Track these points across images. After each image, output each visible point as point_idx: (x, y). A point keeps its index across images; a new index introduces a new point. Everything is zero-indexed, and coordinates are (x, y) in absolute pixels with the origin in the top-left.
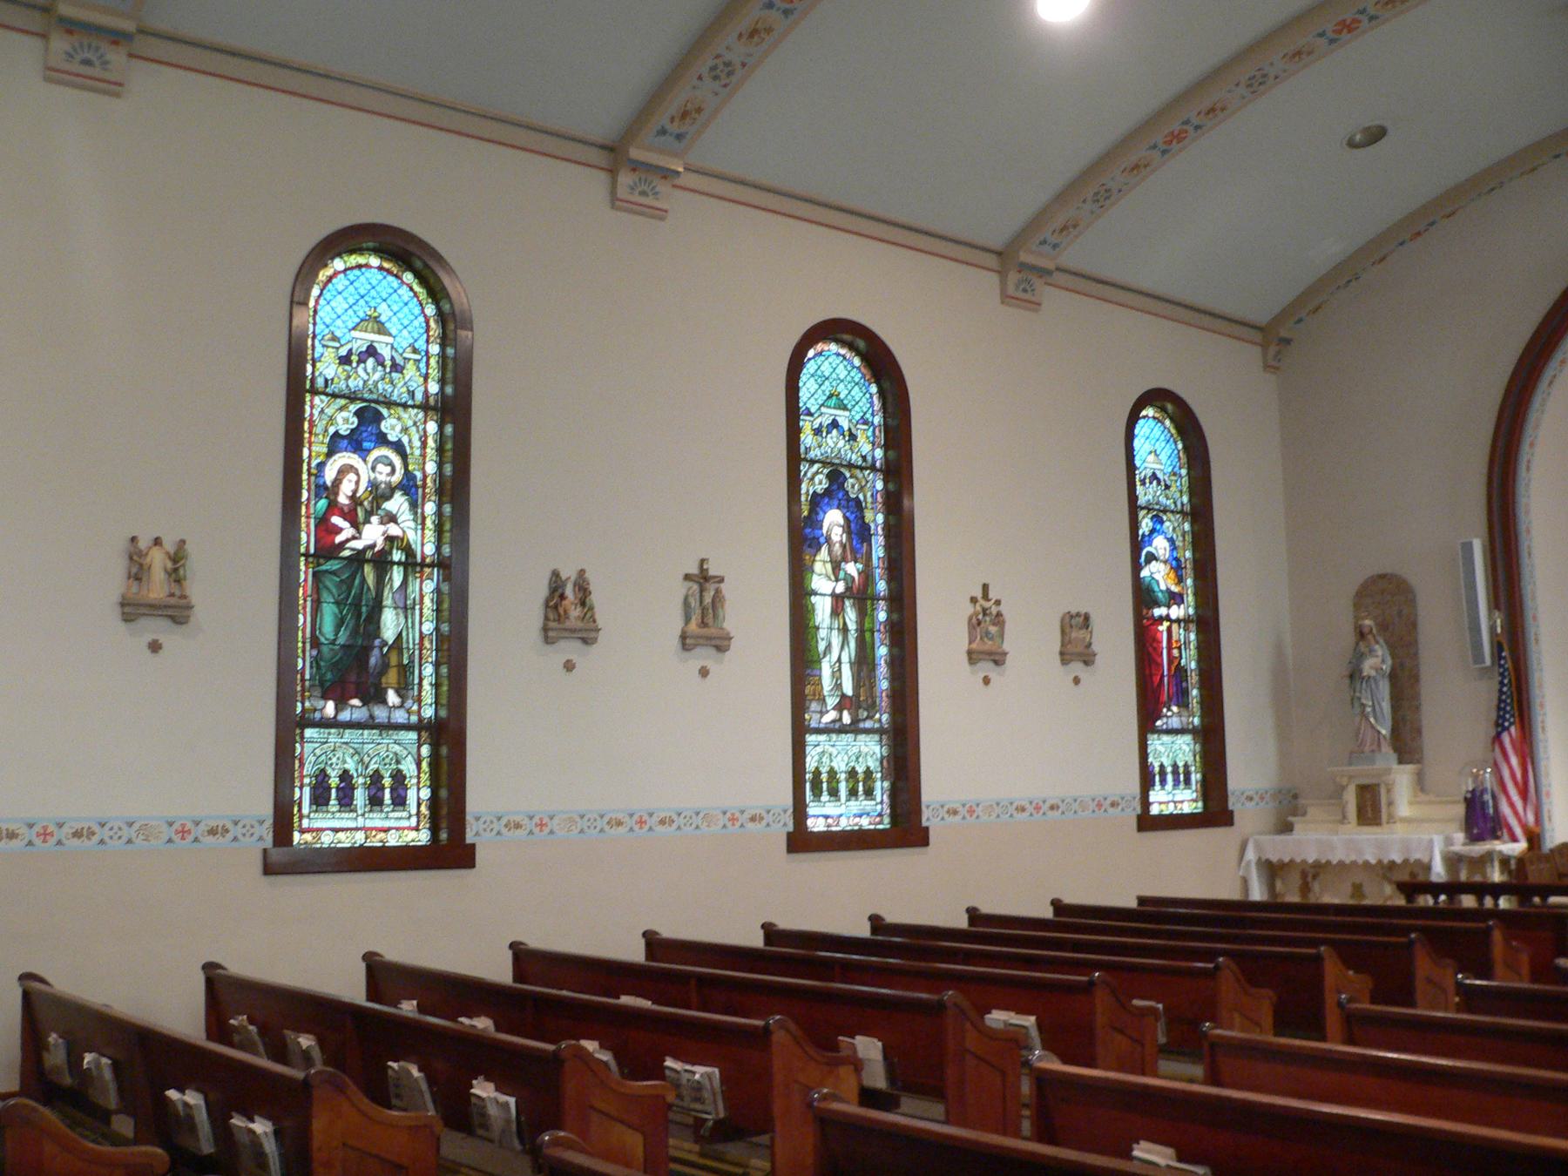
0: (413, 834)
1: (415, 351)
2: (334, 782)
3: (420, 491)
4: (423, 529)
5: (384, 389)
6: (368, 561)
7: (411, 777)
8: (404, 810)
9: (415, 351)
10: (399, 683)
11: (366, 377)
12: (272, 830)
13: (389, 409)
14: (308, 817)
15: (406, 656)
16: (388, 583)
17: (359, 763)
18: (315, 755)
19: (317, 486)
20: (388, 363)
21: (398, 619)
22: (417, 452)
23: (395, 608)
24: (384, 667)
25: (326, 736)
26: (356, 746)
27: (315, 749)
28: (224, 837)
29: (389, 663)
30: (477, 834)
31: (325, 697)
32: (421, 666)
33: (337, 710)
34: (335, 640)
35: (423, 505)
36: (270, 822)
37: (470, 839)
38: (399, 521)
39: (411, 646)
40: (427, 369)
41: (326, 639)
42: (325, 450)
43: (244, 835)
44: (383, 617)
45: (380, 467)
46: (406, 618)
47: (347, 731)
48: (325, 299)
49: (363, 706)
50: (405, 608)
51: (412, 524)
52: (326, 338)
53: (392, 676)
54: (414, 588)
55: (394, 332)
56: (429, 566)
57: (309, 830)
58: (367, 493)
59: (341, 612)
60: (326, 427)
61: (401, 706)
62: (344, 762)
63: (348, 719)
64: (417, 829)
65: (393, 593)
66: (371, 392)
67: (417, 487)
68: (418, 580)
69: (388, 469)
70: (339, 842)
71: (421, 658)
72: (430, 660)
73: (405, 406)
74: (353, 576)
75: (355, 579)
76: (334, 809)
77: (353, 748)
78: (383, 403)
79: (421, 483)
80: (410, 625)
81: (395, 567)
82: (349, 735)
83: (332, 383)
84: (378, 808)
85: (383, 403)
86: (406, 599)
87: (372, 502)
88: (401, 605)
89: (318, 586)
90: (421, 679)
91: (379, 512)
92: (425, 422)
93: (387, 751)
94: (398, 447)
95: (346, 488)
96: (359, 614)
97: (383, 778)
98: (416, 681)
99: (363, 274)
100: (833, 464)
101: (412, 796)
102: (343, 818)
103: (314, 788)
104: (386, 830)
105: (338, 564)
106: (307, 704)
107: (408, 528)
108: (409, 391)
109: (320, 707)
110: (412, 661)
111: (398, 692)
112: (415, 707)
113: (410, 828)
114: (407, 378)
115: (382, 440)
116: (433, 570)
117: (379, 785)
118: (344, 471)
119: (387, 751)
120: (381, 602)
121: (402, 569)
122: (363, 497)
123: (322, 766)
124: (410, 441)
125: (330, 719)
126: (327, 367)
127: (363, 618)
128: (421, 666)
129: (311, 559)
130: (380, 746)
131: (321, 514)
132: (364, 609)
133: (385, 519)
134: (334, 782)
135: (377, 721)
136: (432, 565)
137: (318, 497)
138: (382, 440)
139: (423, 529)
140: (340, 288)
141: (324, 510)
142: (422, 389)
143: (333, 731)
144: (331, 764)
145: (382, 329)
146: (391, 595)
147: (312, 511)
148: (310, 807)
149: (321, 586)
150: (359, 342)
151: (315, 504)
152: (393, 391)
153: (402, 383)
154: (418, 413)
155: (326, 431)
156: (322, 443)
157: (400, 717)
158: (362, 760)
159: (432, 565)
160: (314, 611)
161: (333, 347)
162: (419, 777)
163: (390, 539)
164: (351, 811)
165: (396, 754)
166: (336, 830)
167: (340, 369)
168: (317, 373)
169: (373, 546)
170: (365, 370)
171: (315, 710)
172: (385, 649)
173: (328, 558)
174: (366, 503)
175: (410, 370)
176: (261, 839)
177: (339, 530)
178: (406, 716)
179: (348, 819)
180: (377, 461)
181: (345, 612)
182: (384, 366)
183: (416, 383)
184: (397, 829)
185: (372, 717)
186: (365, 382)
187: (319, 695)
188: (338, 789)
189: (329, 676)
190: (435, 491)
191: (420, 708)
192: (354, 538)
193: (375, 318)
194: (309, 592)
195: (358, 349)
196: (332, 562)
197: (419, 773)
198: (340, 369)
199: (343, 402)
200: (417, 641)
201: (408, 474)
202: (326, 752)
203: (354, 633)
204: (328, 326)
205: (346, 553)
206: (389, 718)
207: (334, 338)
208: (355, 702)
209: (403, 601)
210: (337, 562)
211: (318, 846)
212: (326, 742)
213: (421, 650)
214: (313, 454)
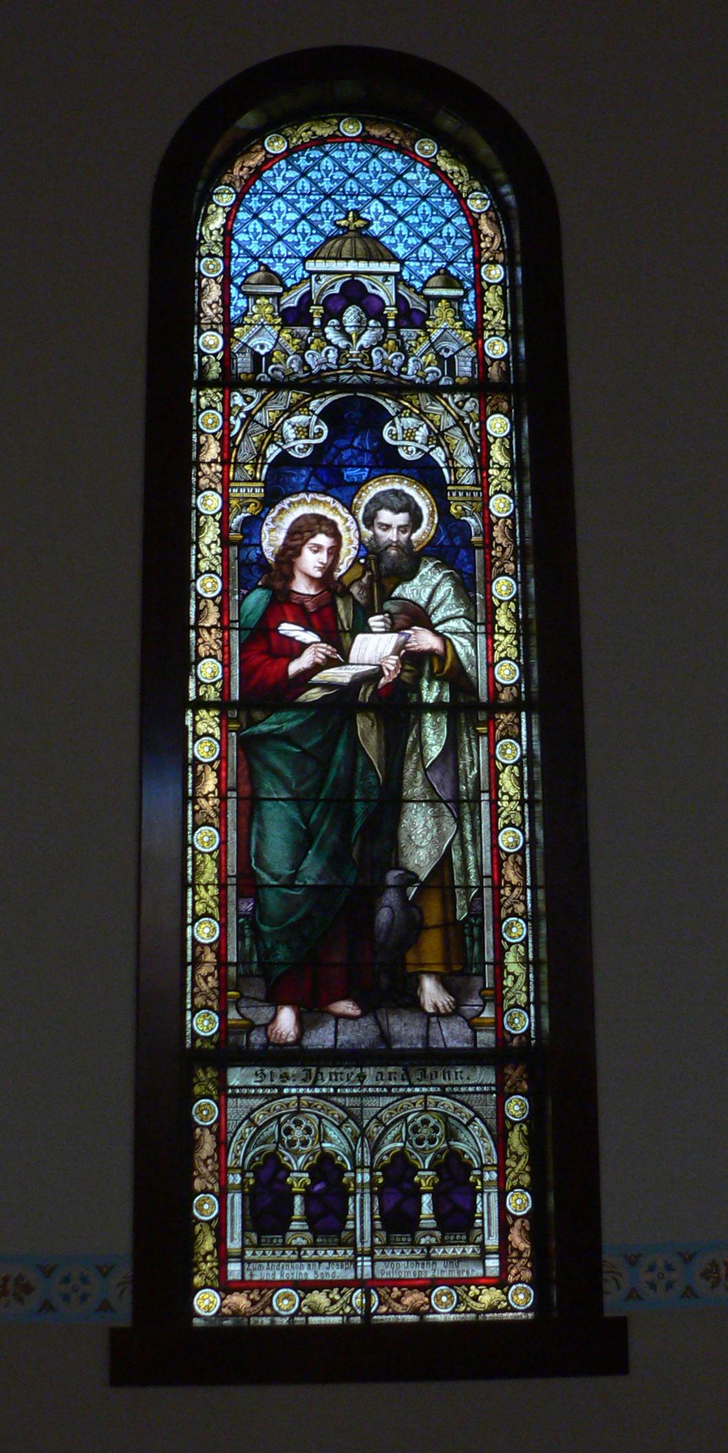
0: (489, 1296)
1: (450, 281)
2: (299, 1179)
3: (479, 555)
4: (490, 634)
5: (383, 362)
6: (365, 708)
7: (482, 1167)
8: (468, 1243)
9: (450, 281)
10: (447, 963)
11: (343, 344)
12: (129, 1287)
13: (396, 399)
14: (241, 1258)
15: (461, 902)
16: (413, 750)
17: (356, 1140)
18: (252, 1122)
19: (243, 564)
20: (391, 312)
21: (439, 826)
22: (468, 478)
23: (432, 803)
24: (412, 928)
25: (276, 1082)
26: (348, 1102)
27: (253, 1111)
28: (21, 1300)
29: (422, 919)
30: (633, 1294)
31: (275, 1000)
32: (498, 922)
33: (303, 1024)
34: (293, 877)
35: (488, 582)
36: (124, 1271)
37: (613, 1302)
38: (435, 620)
39: (473, 880)
40: (480, 312)
41: (274, 876)
42: (259, 493)
43: (66, 1298)
44: (405, 822)
45: (385, 516)
46: (459, 822)
47: (326, 1071)
48: (249, 210)
49: (363, 1015)
50: (456, 802)
51: (462, 625)
52: (253, 280)
53: (432, 945)
54: (475, 758)
55: (400, 251)
56: (506, 708)
57: (242, 1286)
58: (358, 571)
59: (306, 820)
60: (259, 449)
61: (455, 1012)
62: (323, 1137)
63: (329, 1044)
64: (501, 1283)
65: (425, 770)
66: (356, 370)
67: (471, 548)
68: (483, 741)
69: (402, 518)
70: (315, 1313)
71: (497, 907)
72: (520, 908)
73: (434, 390)
74: (330, 743)
75: (336, 743)
76: (299, 1241)
77: (342, 1107)
78: (384, 388)
79: (480, 538)
80: (469, 836)
81: (428, 717)
82: (328, 1080)
83: (269, 363)
84: (406, 1238)
85: (384, 388)
86: (456, 782)
87: (368, 589)
88: (446, 794)
89: (250, 768)
90: (500, 952)
91: (388, 606)
92: (483, 419)
93: (425, 1110)
94: (425, 472)
95: (311, 561)
96: (350, 818)
97: (415, 1170)
98: (489, 956)
99: (327, 154)
100: (339, 387)
101: (487, 1205)
102: (320, 1261)
103: (251, 1198)
104: (427, 1286)
105: (294, 719)
106: (233, 1015)
107: (456, 633)
108: (439, 358)
109: (262, 1021)
110: (476, 913)
111: (445, 983)
112: (488, 1014)
113: (485, 1282)
114: (435, 334)
115: (388, 461)
116: (519, 716)
117: (406, 1186)
118: (301, 532)
119: (425, 1110)
120: (400, 787)
121: (443, 720)
122: (346, 581)
123: (271, 1147)
124: (450, 458)
125: (287, 1044)
126: (257, 334)
127: (359, 824)
128: (498, 922)
129: (234, 714)
130: (406, 1102)
131: (254, 619)
132: (359, 809)
133: (400, 621)
134: (299, 1179)
135: (397, 1046)
136: (514, 707)
137: (247, 586)
138: (388, 461)
139: (490, 634)
140: (280, 185)
141: (260, 610)
142: (472, 352)
143: (291, 1071)
144: (292, 1143)
145: (375, 250)
146: (420, 776)
147: (234, 615)
148: (243, 1237)
149: (257, 766)
150: (324, 280)
151: (240, 603)
152: (405, 364)
153: (426, 344)
154: (465, 401)
155: (261, 454)
156: (254, 480)
157: (453, 1035)
158: (363, 1132)
159: (514, 707)
160: (244, 820)
161: (267, 296)
162: (501, 1168)
163: (412, 659)
164: (342, 1244)
165: (445, 1116)
166: (305, 1287)
167: (285, 335)
168: (235, 348)
169: (379, 673)
170: (341, 329)
171: (252, 1027)
172: (412, 892)
173: (271, 709)
174: (355, 590)
175: (442, 318)
176: (105, 1306)
177: (298, 648)
178: (468, 1033)
179: (330, 1261)
180: (378, 503)
181: (314, 817)
182: (383, 320)
183: (457, 341)
184: (452, 1283)
185: (385, 1037)
186: (340, 351)
187: (261, 996)
188: (308, 1195)
189: (281, 954)
190: (514, 554)
191: (500, 1013)
192: (330, 663)
193: (358, 229)
194: (232, 781)
195: (321, 294)
196: (283, 715)
197: (502, 1156)
198: (285, 335)
199: (294, 396)
200: (487, 870)
201: (448, 523)
202: (279, 1117)
203: (337, 860)
204: (255, 258)
205: (314, 694)
206: (426, 1039)
207: (271, 277)
208: (346, 1007)
209: (449, 785)
210: (291, 715)
211: (266, 1321)
212: (281, 1096)
213: (496, 889)
214: (233, 502)
